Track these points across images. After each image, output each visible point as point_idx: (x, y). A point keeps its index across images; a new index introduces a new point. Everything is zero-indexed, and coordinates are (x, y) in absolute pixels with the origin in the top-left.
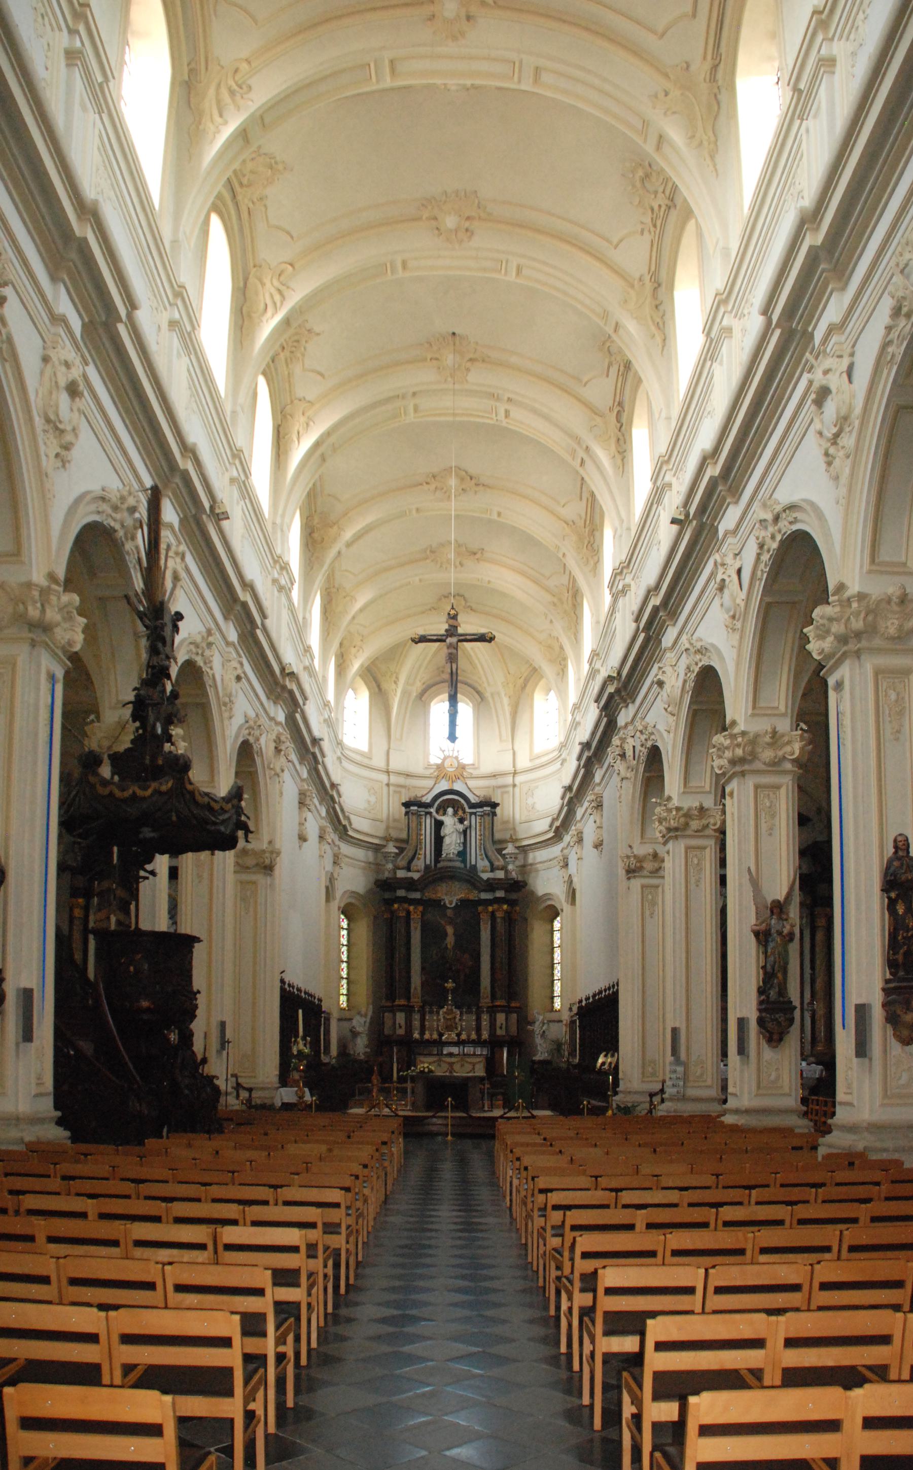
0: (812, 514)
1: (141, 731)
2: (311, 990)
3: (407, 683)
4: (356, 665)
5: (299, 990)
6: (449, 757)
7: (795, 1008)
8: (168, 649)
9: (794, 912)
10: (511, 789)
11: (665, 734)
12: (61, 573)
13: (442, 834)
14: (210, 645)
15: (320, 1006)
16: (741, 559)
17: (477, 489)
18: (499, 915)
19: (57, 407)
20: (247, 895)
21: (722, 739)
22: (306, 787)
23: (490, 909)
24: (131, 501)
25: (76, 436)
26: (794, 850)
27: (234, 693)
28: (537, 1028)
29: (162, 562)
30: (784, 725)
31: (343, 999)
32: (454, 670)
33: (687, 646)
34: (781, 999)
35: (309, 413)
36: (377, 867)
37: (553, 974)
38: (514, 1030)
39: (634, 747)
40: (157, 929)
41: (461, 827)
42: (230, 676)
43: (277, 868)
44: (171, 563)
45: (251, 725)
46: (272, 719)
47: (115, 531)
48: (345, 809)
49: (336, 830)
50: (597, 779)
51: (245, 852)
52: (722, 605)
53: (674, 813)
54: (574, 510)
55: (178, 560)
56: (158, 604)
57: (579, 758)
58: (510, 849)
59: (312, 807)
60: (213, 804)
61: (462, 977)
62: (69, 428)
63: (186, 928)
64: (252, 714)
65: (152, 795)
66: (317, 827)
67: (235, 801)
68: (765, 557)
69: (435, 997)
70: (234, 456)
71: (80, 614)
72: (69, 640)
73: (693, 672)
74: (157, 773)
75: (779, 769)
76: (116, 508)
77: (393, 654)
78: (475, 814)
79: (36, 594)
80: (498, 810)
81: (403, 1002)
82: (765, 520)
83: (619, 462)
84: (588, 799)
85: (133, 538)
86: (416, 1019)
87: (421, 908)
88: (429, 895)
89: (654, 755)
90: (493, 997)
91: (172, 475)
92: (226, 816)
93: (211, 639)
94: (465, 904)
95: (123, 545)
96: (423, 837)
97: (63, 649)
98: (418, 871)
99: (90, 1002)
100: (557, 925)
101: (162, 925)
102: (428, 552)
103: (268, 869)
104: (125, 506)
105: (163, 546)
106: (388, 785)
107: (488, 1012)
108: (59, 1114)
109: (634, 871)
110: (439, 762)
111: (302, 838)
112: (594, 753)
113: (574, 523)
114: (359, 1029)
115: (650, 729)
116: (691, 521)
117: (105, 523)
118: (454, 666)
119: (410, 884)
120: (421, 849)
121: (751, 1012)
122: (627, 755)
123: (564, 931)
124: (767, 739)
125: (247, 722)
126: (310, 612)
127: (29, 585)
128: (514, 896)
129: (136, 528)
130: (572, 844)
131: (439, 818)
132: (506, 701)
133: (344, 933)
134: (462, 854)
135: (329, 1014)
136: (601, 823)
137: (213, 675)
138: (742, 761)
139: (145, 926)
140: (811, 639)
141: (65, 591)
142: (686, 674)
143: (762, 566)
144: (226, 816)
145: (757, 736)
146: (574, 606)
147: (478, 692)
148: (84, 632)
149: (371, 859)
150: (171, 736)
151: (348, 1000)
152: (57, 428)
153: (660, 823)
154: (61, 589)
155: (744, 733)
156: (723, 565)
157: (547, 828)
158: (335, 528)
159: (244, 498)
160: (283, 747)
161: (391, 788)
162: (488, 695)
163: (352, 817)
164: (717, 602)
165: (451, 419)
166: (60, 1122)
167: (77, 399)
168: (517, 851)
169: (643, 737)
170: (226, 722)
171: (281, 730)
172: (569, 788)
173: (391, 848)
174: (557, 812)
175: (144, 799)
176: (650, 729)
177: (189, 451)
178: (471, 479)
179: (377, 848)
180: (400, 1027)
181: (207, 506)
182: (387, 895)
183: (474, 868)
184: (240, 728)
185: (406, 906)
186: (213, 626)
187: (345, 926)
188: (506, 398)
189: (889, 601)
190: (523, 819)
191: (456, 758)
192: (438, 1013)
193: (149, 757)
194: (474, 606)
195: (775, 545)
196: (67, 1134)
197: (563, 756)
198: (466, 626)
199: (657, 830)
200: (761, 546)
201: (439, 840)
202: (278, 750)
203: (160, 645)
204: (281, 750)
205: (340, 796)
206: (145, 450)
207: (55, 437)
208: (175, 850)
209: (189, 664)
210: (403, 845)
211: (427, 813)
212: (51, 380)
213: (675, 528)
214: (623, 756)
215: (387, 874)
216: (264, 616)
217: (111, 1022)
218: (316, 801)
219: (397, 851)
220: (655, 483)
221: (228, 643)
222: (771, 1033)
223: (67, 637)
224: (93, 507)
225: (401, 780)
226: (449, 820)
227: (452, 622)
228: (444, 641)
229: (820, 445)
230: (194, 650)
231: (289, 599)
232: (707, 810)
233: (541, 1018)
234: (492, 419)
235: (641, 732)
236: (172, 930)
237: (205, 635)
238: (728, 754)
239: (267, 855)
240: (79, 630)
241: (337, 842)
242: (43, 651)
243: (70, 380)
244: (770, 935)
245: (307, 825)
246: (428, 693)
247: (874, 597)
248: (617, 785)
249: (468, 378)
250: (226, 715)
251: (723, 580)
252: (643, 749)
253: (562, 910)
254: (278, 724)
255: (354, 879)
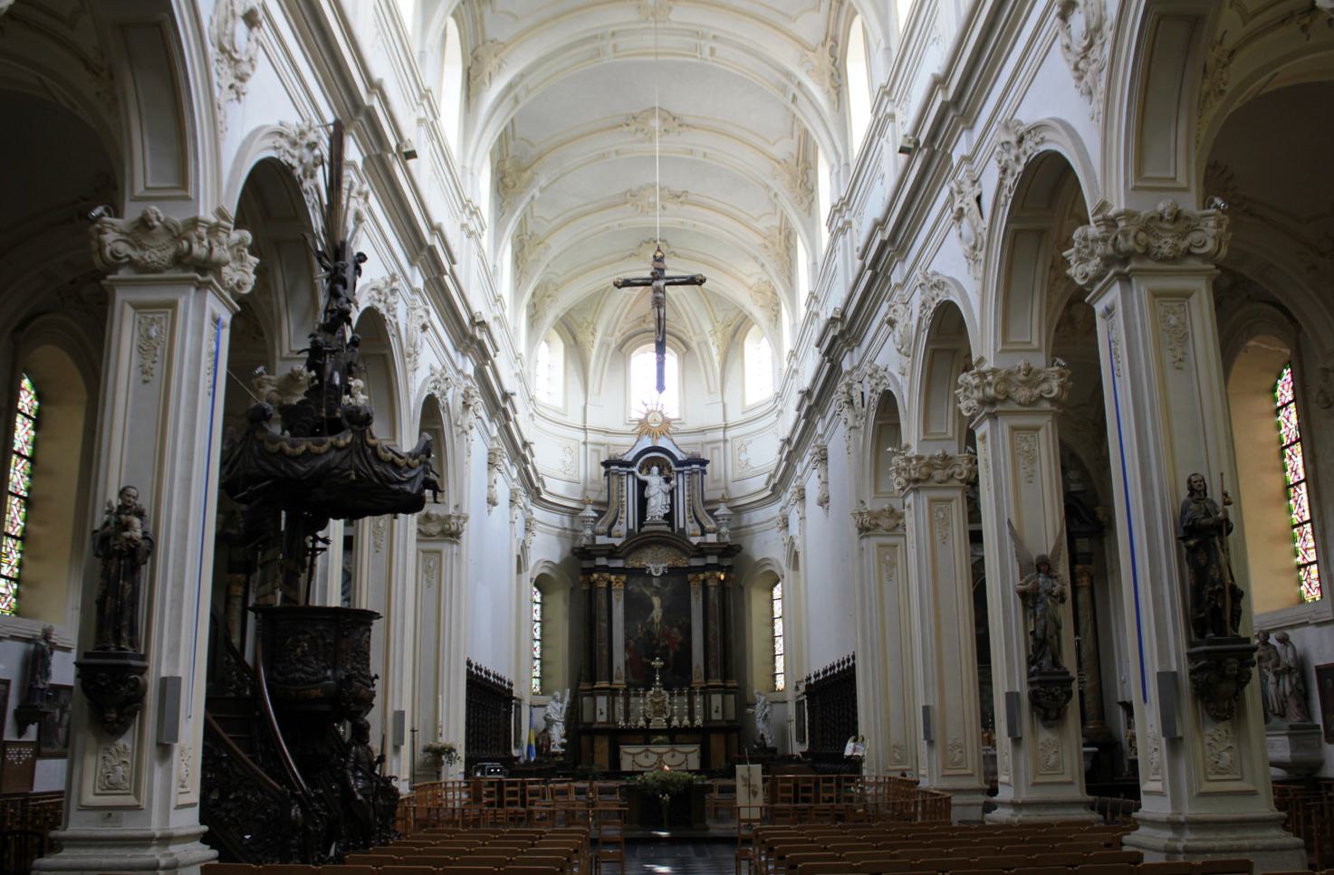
0: (1064, 133)
1: (317, 382)
2: (501, 673)
3: (605, 334)
4: (552, 314)
5: (487, 673)
6: (652, 411)
7: (1072, 680)
8: (348, 291)
9: (1063, 569)
10: (722, 444)
11: (899, 377)
12: (232, 210)
13: (646, 496)
14: (393, 291)
15: (510, 691)
16: (980, 186)
17: (680, 129)
18: (711, 583)
19: (233, 35)
20: (432, 567)
21: (970, 378)
22: (496, 446)
23: (702, 577)
24: (312, 137)
25: (253, 67)
26: (1059, 500)
27: (419, 343)
28: (759, 711)
29: (344, 202)
30: (1039, 361)
31: (536, 682)
32: (662, 316)
33: (922, 280)
34: (1056, 670)
35: (503, 55)
36: (575, 533)
37: (774, 649)
38: (731, 715)
39: (862, 393)
40: (328, 605)
41: (666, 487)
42: (417, 325)
43: (464, 535)
44: (353, 204)
45: (440, 379)
46: (459, 372)
47: (293, 168)
48: (539, 470)
49: (528, 493)
50: (820, 430)
51: (428, 518)
52: (960, 235)
53: (914, 462)
54: (785, 148)
55: (361, 200)
56: (339, 244)
57: (799, 409)
58: (722, 510)
59: (502, 468)
60: (397, 459)
61: (671, 653)
62: (245, 58)
63: (365, 602)
64: (438, 367)
65: (327, 452)
66: (508, 490)
67: (423, 457)
68: (1009, 181)
69: (641, 677)
70: (422, 97)
71: (252, 253)
72: (238, 282)
73: (930, 308)
74: (335, 427)
75: (1037, 409)
76: (294, 144)
77: (594, 301)
78: (682, 472)
79: (203, 231)
80: (708, 467)
81: (604, 684)
82: (1008, 143)
83: (834, 97)
84: (810, 451)
85: (313, 176)
86: (699, 703)
87: (624, 578)
88: (633, 563)
89: (887, 403)
90: (707, 676)
91: (355, 109)
92: (412, 473)
93: (395, 285)
94: (673, 571)
95: (301, 182)
96: (625, 499)
97: (233, 294)
98: (620, 537)
99: (248, 693)
100: (777, 592)
101: (335, 600)
102: (628, 196)
103: (453, 535)
104: (304, 142)
105: (345, 186)
106: (585, 443)
107: (701, 693)
108: (205, 828)
109: (868, 529)
110: (642, 417)
111: (492, 502)
112: (815, 403)
113: (786, 162)
114: (554, 717)
115: (881, 373)
116: (920, 150)
117: (282, 159)
118: (662, 311)
119: (611, 552)
120: (622, 512)
121: (1021, 686)
122: (855, 402)
123: (786, 598)
124: (1021, 377)
125: (432, 375)
126: (501, 260)
127: (195, 222)
128: (727, 562)
129: (316, 165)
130: (792, 502)
131: (642, 477)
132: (714, 351)
133: (537, 607)
134: (669, 517)
135: (520, 700)
136: (827, 478)
137: (397, 324)
138: (993, 402)
139: (316, 601)
140: (1072, 263)
141: (235, 228)
142: (921, 312)
143: (1006, 191)
144: (412, 473)
145: (1010, 373)
146: (787, 248)
147: (683, 342)
148: (255, 273)
149: (567, 525)
150: (350, 387)
151: (541, 684)
152: (232, 58)
153: (899, 474)
154: (232, 226)
155: (994, 371)
156: (960, 192)
157: (763, 485)
158: (529, 172)
159: (432, 139)
160: (472, 403)
161: (589, 447)
162: (694, 345)
163: (545, 478)
164: (954, 231)
165: (652, 58)
166: (205, 839)
167: (255, 29)
168: (730, 513)
169: (874, 382)
170: (410, 374)
171: (470, 384)
172: (788, 441)
173: (590, 512)
174: (774, 467)
175: (319, 455)
176: (881, 373)
177: (375, 87)
178: (674, 119)
179: (573, 513)
180: (602, 713)
181: (393, 144)
182: (586, 564)
183: (682, 531)
184: (425, 381)
185: (606, 575)
186: (397, 271)
187: (538, 600)
188: (711, 36)
189: (1162, 218)
190: (736, 477)
191: (660, 412)
192: (644, 695)
193: (322, 411)
194: (677, 251)
195: (1020, 168)
196: (215, 853)
197: (779, 408)
198: (674, 269)
199: (896, 481)
200: (1004, 171)
201: (643, 503)
202: (466, 406)
203: (340, 288)
204: (469, 406)
205: (533, 456)
206: (327, 87)
207: (230, 67)
208: (352, 515)
209: (371, 316)
210: (603, 509)
211: (629, 473)
212: (227, 8)
213: (903, 158)
214: (850, 402)
215: (584, 541)
216: (453, 262)
217: (272, 713)
218: (506, 461)
219: (596, 515)
220: (876, 115)
221: (414, 291)
222: (1047, 710)
223: (237, 277)
224: (269, 142)
225: (601, 438)
226: (655, 481)
227: (657, 264)
228: (650, 285)
229: (1068, 61)
230: (377, 297)
231: (479, 246)
232: (951, 458)
233: (763, 698)
234: (695, 57)
235: (871, 376)
236: (346, 605)
237: (389, 280)
238: (978, 394)
239: (453, 520)
240: (251, 270)
241: (530, 507)
242: (209, 293)
243: (248, 8)
244: (1038, 594)
245: (497, 487)
246: (627, 345)
247: (1143, 214)
248: (841, 435)
249: (671, 17)
250: (410, 367)
251: (961, 209)
252: (874, 395)
253: (783, 577)
254: (466, 377)
255: (546, 549)
